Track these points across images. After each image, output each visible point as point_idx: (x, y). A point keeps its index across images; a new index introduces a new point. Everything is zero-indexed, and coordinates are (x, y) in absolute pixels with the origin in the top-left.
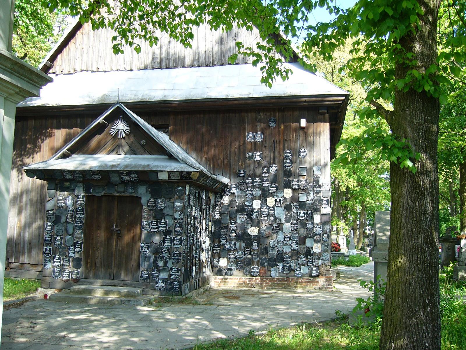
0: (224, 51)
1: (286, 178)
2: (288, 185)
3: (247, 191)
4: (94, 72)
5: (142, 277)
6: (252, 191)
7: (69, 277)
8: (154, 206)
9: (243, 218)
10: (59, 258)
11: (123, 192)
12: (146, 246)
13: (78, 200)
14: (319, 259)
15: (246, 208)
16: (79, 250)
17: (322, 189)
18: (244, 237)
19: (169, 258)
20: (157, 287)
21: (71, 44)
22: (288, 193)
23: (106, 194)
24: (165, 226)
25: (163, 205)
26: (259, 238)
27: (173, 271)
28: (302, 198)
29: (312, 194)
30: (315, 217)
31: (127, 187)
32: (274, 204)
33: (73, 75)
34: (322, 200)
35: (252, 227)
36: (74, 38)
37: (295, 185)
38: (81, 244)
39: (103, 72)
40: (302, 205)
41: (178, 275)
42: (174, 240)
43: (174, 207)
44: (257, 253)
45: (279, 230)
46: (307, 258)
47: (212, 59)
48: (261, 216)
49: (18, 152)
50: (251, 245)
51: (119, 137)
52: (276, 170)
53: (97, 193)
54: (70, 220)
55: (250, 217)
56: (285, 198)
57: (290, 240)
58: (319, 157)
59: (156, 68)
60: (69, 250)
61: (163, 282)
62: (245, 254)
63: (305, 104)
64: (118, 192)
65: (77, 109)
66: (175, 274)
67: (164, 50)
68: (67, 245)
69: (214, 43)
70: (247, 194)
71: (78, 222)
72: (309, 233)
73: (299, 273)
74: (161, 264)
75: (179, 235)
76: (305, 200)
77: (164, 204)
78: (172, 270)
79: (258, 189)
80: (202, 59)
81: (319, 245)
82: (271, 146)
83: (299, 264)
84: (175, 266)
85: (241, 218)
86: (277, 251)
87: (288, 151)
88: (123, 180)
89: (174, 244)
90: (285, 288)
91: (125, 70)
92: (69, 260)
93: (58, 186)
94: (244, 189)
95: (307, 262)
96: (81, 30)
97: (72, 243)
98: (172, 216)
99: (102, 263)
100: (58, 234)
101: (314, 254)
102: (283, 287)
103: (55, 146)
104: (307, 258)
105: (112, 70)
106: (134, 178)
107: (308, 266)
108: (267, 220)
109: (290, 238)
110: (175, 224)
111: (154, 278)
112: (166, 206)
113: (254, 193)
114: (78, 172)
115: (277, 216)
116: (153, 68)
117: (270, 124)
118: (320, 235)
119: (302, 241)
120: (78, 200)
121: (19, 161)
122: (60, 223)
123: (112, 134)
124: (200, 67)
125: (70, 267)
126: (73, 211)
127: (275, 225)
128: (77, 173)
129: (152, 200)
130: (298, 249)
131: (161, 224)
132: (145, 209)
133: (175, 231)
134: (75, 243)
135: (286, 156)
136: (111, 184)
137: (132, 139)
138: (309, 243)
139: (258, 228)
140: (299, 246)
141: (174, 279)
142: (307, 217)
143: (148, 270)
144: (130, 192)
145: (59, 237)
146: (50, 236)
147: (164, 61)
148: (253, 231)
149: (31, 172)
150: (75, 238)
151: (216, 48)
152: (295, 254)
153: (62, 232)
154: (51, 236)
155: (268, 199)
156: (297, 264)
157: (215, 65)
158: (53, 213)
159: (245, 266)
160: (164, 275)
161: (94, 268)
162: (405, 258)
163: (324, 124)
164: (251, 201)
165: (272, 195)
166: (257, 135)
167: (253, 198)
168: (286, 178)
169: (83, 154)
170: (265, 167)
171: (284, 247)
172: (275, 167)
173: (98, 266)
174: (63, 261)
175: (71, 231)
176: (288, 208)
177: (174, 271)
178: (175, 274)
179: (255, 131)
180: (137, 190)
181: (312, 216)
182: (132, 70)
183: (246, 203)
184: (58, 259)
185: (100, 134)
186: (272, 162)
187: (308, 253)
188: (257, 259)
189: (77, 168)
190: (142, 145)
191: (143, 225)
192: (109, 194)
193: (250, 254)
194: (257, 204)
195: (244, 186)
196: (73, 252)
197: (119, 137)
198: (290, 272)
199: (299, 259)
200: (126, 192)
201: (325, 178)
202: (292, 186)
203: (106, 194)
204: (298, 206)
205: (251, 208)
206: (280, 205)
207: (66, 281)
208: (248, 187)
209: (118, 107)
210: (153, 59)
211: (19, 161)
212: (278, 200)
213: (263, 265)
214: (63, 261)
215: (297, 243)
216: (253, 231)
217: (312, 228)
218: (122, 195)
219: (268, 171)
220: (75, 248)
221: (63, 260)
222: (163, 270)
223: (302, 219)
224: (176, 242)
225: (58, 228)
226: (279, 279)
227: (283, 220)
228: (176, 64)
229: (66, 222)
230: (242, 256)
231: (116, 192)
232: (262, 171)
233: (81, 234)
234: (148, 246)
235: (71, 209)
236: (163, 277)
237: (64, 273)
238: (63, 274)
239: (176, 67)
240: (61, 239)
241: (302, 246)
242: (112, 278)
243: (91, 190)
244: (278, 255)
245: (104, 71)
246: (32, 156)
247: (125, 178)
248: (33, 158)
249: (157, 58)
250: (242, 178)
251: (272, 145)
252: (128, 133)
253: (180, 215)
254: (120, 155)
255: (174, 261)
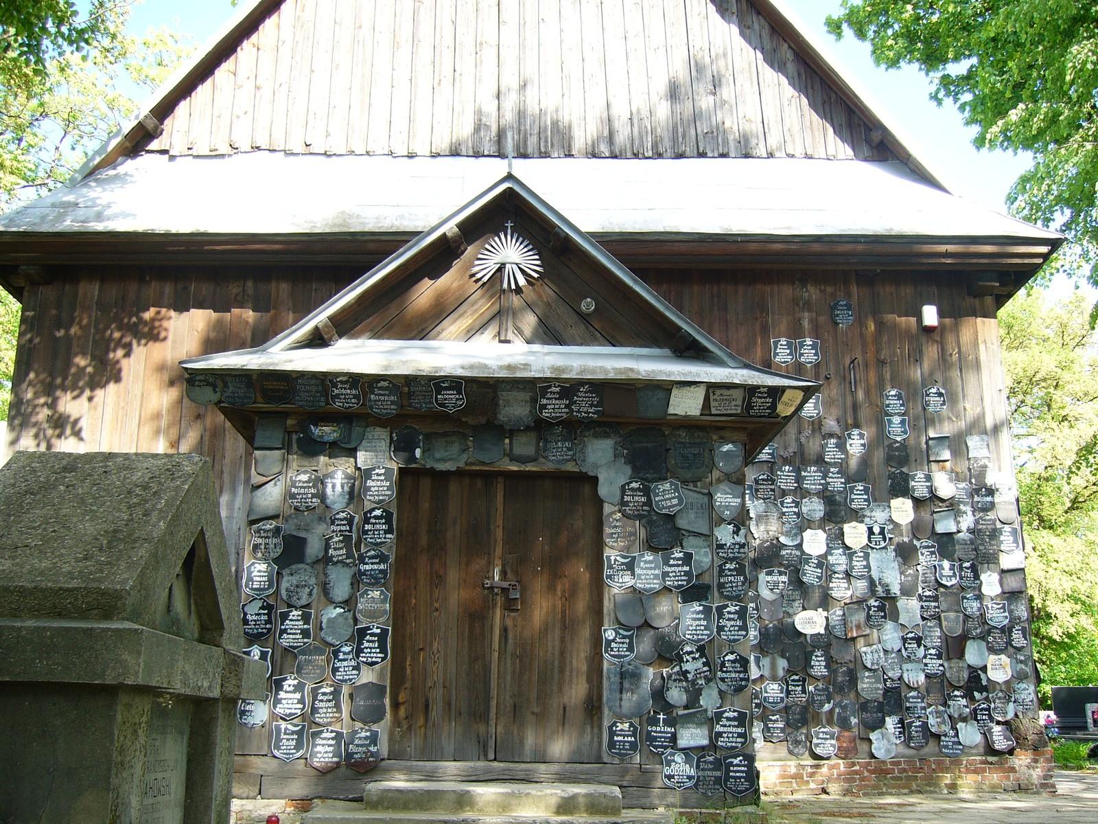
0: (685, 120)
1: (893, 472)
2: (901, 488)
3: (782, 503)
4: (293, 154)
5: (612, 744)
6: (797, 504)
7: (337, 754)
8: (644, 504)
9: (776, 584)
10: (299, 688)
11: (533, 460)
12: (624, 637)
13: (369, 483)
14: (1008, 699)
15: (784, 552)
16: (377, 656)
17: (997, 498)
18: (782, 639)
19: (706, 677)
20: (670, 777)
21: (223, 72)
22: (902, 511)
23: (472, 464)
24: (687, 569)
25: (675, 501)
26: (826, 642)
27: (724, 722)
28: (945, 525)
29: (970, 513)
30: (983, 577)
31: (546, 441)
32: (865, 541)
33: (227, 159)
34: (1000, 531)
35: (804, 609)
36: (232, 58)
37: (919, 487)
38: (382, 637)
39: (323, 158)
40: (945, 544)
41: (740, 735)
42: (721, 615)
43: (711, 506)
44: (827, 689)
45: (884, 617)
46: (972, 699)
47: (650, 139)
48: (829, 578)
49: (42, 377)
50: (807, 664)
51: (505, 285)
52: (863, 445)
53: (439, 460)
54: (338, 553)
55: (797, 582)
56: (897, 525)
57: (919, 647)
58: (979, 410)
59: (486, 153)
60: (336, 657)
61: (688, 761)
62: (788, 693)
63: (943, 260)
64: (514, 459)
65: (258, 246)
66: (731, 729)
67: (510, 104)
68: (329, 639)
69: (654, 99)
70: (784, 514)
71: (371, 558)
72: (970, 624)
73: (954, 743)
74: (676, 695)
75: (738, 598)
76: (954, 530)
77: (679, 498)
78: (719, 716)
79: (815, 499)
80: (622, 137)
81: (1004, 658)
82: (844, 378)
83: (950, 717)
84: (728, 702)
85: (769, 585)
86: (885, 681)
87: (893, 393)
88: (545, 414)
89: (721, 629)
90: (920, 792)
91: (391, 154)
92: (336, 694)
93: (294, 437)
94: (775, 499)
95: (975, 710)
96: (254, 38)
97: (347, 633)
98: (708, 536)
99: (449, 704)
100: (294, 600)
101: (991, 689)
102: (914, 787)
103: (169, 362)
104: (972, 699)
105: (352, 153)
106: (585, 407)
107: (978, 721)
108: (848, 589)
109: (918, 640)
110: (717, 562)
111: (656, 747)
112: (685, 507)
113: (804, 510)
114: (385, 384)
115: (875, 574)
116: (477, 155)
117: (838, 315)
118: (1002, 630)
119: (954, 647)
120: (369, 483)
121: (43, 406)
122: (302, 561)
123: (479, 276)
124: (616, 157)
125: (340, 720)
126: (350, 521)
127: (872, 602)
128: (381, 388)
129: (634, 485)
130: (944, 674)
131: (672, 562)
132: (614, 513)
133: (721, 586)
134: (362, 633)
135: (888, 406)
136: (497, 431)
137: (548, 292)
138: (973, 654)
139: (825, 614)
140: (946, 665)
141: (727, 748)
142: (961, 578)
143: (636, 721)
144: (557, 457)
145: (295, 613)
146: (262, 608)
147: (509, 135)
148: (810, 621)
149: (209, 384)
150: (359, 616)
151: (663, 111)
152: (939, 686)
153: (310, 594)
154: (269, 608)
155: (847, 528)
156: (946, 717)
157: (660, 156)
158: (277, 531)
159: (790, 730)
160: (692, 736)
161: (421, 721)
162: (494, 797)
163: (984, 323)
164: (796, 535)
165: (857, 516)
166: (802, 345)
167: (804, 524)
168: (893, 472)
169: (378, 338)
170: (831, 435)
171: (905, 666)
172: (861, 436)
173: (436, 712)
174: (315, 699)
175: (341, 590)
176: (906, 554)
177: (728, 719)
178: (731, 729)
179: (795, 333)
180: (582, 451)
181: (977, 577)
182: (411, 156)
183: (783, 540)
184: (294, 692)
185: (435, 276)
186: (850, 421)
187: (975, 682)
188: (827, 707)
189: (386, 367)
190: (583, 317)
191: (610, 567)
192: (483, 463)
193: (804, 691)
194: (815, 542)
195: (773, 490)
196: (353, 663)
197: (505, 285)
198: (927, 744)
199: (951, 703)
200: (541, 459)
201: (1000, 470)
202: (914, 490)
203: (472, 464)
204: (933, 546)
205: (798, 553)
206: (883, 544)
207: (324, 773)
208: (784, 493)
209: (510, 188)
210: (477, 129)
211: (43, 406)
212: (876, 530)
213: (844, 724)
214: (315, 699)
215: (939, 656)
216: (810, 622)
217: (979, 609)
218: (530, 467)
219: (841, 446)
220: (359, 651)
221: (315, 692)
222: (688, 720)
223: (949, 584)
224: (729, 624)
225: (294, 580)
226: (899, 763)
227: (895, 589)
228: (546, 146)
229: (326, 560)
230: (782, 699)
231: (507, 460)
232: (823, 447)
233: (384, 601)
234: (630, 637)
235: (342, 515)
236: (693, 743)
237: (319, 741)
238: (314, 745)
239: (545, 155)
240: (306, 618)
241: (954, 663)
242: (491, 756)
243: (418, 453)
244: (887, 691)
245: (325, 154)
246: (87, 393)
247: (554, 408)
248: (90, 399)
249: (488, 127)
250: (765, 467)
251: (847, 375)
252: (536, 275)
253: (736, 532)
254: (508, 342)
255: (723, 687)
